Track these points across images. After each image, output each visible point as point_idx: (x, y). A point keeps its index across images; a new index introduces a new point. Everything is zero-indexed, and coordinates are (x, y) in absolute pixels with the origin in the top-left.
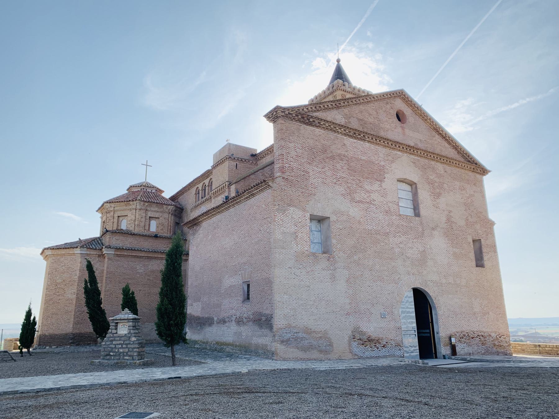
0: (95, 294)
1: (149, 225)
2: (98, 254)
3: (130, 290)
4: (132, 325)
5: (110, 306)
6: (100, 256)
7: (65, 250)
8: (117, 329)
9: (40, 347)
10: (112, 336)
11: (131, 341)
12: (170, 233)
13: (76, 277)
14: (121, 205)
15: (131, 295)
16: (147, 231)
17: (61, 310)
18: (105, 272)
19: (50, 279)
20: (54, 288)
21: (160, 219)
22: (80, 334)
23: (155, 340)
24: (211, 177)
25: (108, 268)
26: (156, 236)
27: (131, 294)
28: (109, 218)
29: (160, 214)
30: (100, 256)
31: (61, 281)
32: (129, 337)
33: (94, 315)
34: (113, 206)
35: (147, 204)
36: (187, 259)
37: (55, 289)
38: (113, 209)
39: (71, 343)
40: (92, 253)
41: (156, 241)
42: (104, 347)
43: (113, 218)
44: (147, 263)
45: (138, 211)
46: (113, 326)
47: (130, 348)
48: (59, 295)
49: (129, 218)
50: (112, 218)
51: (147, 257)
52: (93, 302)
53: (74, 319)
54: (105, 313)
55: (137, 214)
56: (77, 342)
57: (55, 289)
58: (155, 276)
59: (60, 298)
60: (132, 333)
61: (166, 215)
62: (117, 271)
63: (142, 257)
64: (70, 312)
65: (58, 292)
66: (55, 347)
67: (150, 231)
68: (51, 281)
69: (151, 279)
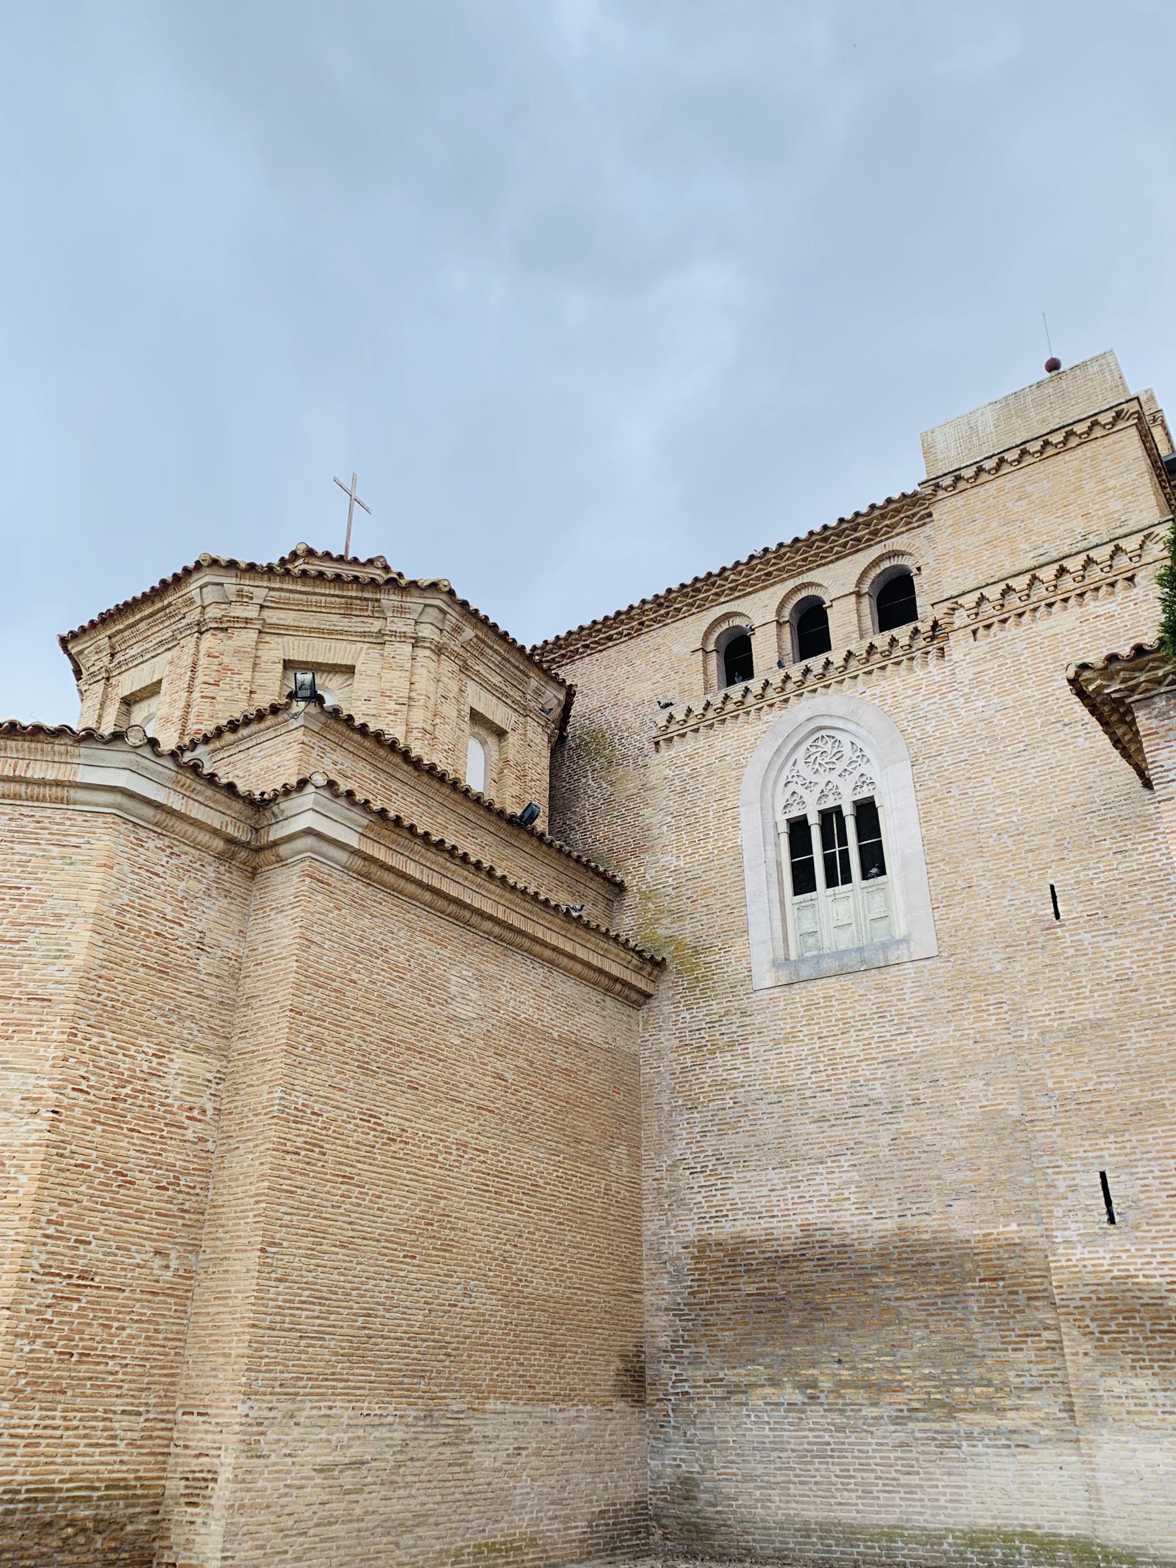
2: (230, 830)
13: (62, 971)
14: (314, 598)
22: (43, 1493)
23: (532, 1542)
24: (897, 543)
30: (232, 857)
40: (197, 812)
41: (508, 851)
45: (428, 653)
50: (249, 664)
58: (525, 1065)
62: (355, 976)
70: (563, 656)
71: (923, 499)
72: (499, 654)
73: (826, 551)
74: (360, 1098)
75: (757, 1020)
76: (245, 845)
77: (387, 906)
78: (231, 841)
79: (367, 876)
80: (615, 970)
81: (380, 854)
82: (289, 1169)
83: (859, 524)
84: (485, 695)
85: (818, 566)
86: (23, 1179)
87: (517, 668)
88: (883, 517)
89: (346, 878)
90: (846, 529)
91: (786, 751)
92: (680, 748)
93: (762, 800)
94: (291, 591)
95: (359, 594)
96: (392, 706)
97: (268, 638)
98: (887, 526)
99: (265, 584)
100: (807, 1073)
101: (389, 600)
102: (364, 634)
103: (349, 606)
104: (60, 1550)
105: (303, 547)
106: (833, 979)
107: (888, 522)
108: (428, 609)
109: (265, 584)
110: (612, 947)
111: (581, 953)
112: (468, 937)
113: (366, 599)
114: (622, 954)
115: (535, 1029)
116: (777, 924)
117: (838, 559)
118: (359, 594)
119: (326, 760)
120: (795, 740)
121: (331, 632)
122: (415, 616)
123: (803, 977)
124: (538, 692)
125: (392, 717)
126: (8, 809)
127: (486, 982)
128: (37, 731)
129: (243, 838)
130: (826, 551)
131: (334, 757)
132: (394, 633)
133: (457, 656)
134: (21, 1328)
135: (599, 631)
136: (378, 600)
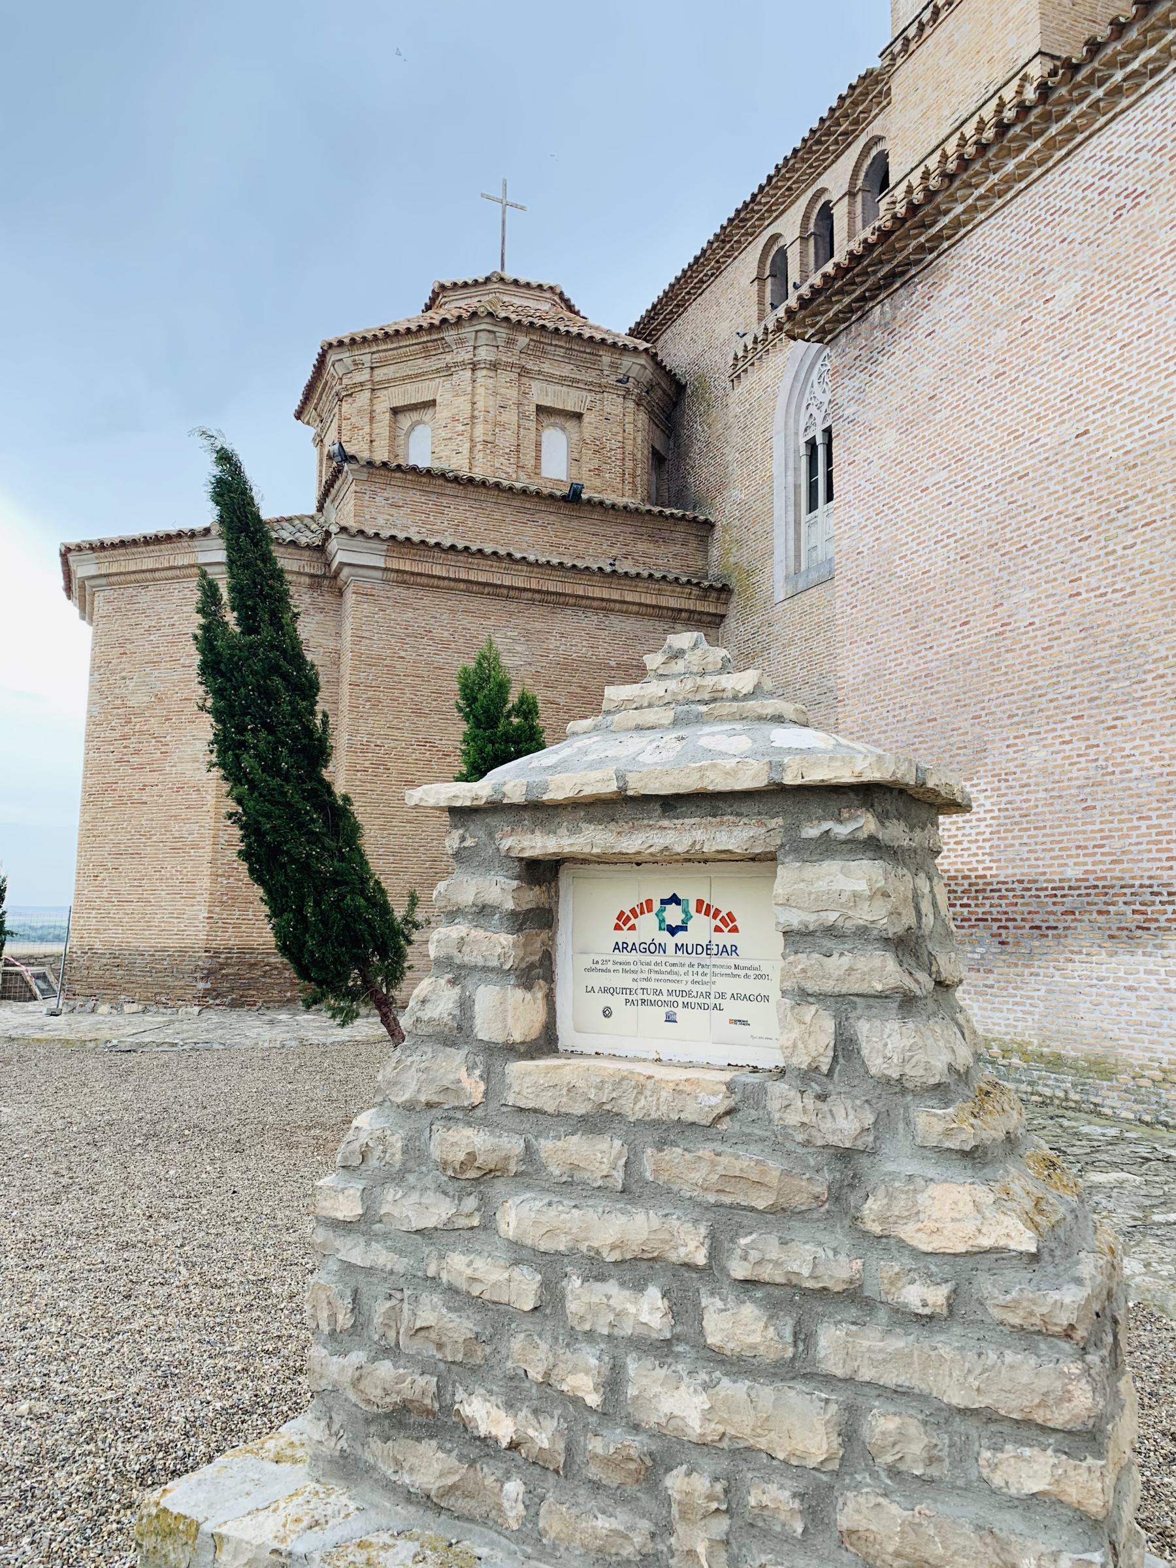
0: (277, 680)
1: (538, 445)
2: (307, 570)
3: (503, 687)
4: (874, 914)
5: (378, 822)
6: (320, 586)
7: (151, 548)
8: (549, 977)
9: (71, 1003)
10: (474, 1089)
11: (884, 1243)
12: (635, 491)
14: (401, 350)
15: (515, 721)
16: (529, 477)
17: (154, 838)
18: (347, 658)
19: (101, 693)
20: (116, 734)
21: (586, 419)
24: (874, 129)
25: (358, 638)
26: (573, 498)
27: (516, 710)
28: (353, 420)
29: (584, 393)
30: (320, 586)
31: (146, 699)
32: (844, 1155)
33: (275, 829)
34: (367, 359)
35: (527, 340)
36: (723, 616)
37: (124, 737)
38: (367, 377)
39: (207, 993)
41: (575, 523)
42: (348, 1268)
43: (372, 419)
44: (538, 625)
45: (484, 372)
46: (482, 912)
47: (899, 1393)
48: (141, 767)
49: (442, 413)
50: (367, 419)
51: (537, 596)
52: (263, 734)
53: (214, 881)
54: (356, 829)
55: (481, 391)
56: (232, 989)
57: (124, 737)
58: (578, 690)
59: (149, 781)
60: (898, 1087)
61: (614, 404)
62: (402, 654)
63: (517, 593)
64: (195, 847)
65: (137, 752)
66: (135, 1007)
67: (544, 474)
68: (105, 702)
69: (562, 701)
70: (677, 306)
71: (880, 74)
72: (561, 347)
73: (824, 153)
74: (415, 731)
75: (776, 628)
76: (324, 576)
77: (428, 599)
78: (312, 576)
79: (405, 582)
80: (673, 603)
81: (407, 566)
82: (360, 780)
83: (838, 118)
84: (552, 388)
85: (825, 169)
86: (209, 798)
87: (585, 352)
88: (855, 104)
89: (388, 588)
90: (830, 126)
91: (803, 375)
92: (747, 381)
93: (786, 429)
94: (385, 350)
95: (429, 338)
96: (460, 428)
97: (378, 393)
98: (861, 112)
99: (367, 350)
100: (797, 669)
101: (450, 335)
102: (438, 371)
103: (426, 350)
104: (263, 977)
105: (437, 285)
106: (814, 590)
107: (861, 108)
108: (479, 334)
109: (367, 350)
110: (664, 586)
111: (629, 597)
112: (513, 607)
113: (435, 340)
114: (678, 589)
115: (591, 663)
116: (791, 544)
117: (837, 157)
118: (429, 338)
119: (378, 499)
120: (808, 363)
121: (417, 375)
122: (472, 343)
123: (800, 588)
124: (614, 366)
125: (460, 438)
126: (177, 586)
127: (533, 637)
128: (168, 538)
129: (319, 573)
130: (824, 153)
131: (385, 495)
132: (456, 364)
133: (513, 365)
134: (220, 872)
135: (691, 277)
136: (443, 338)
